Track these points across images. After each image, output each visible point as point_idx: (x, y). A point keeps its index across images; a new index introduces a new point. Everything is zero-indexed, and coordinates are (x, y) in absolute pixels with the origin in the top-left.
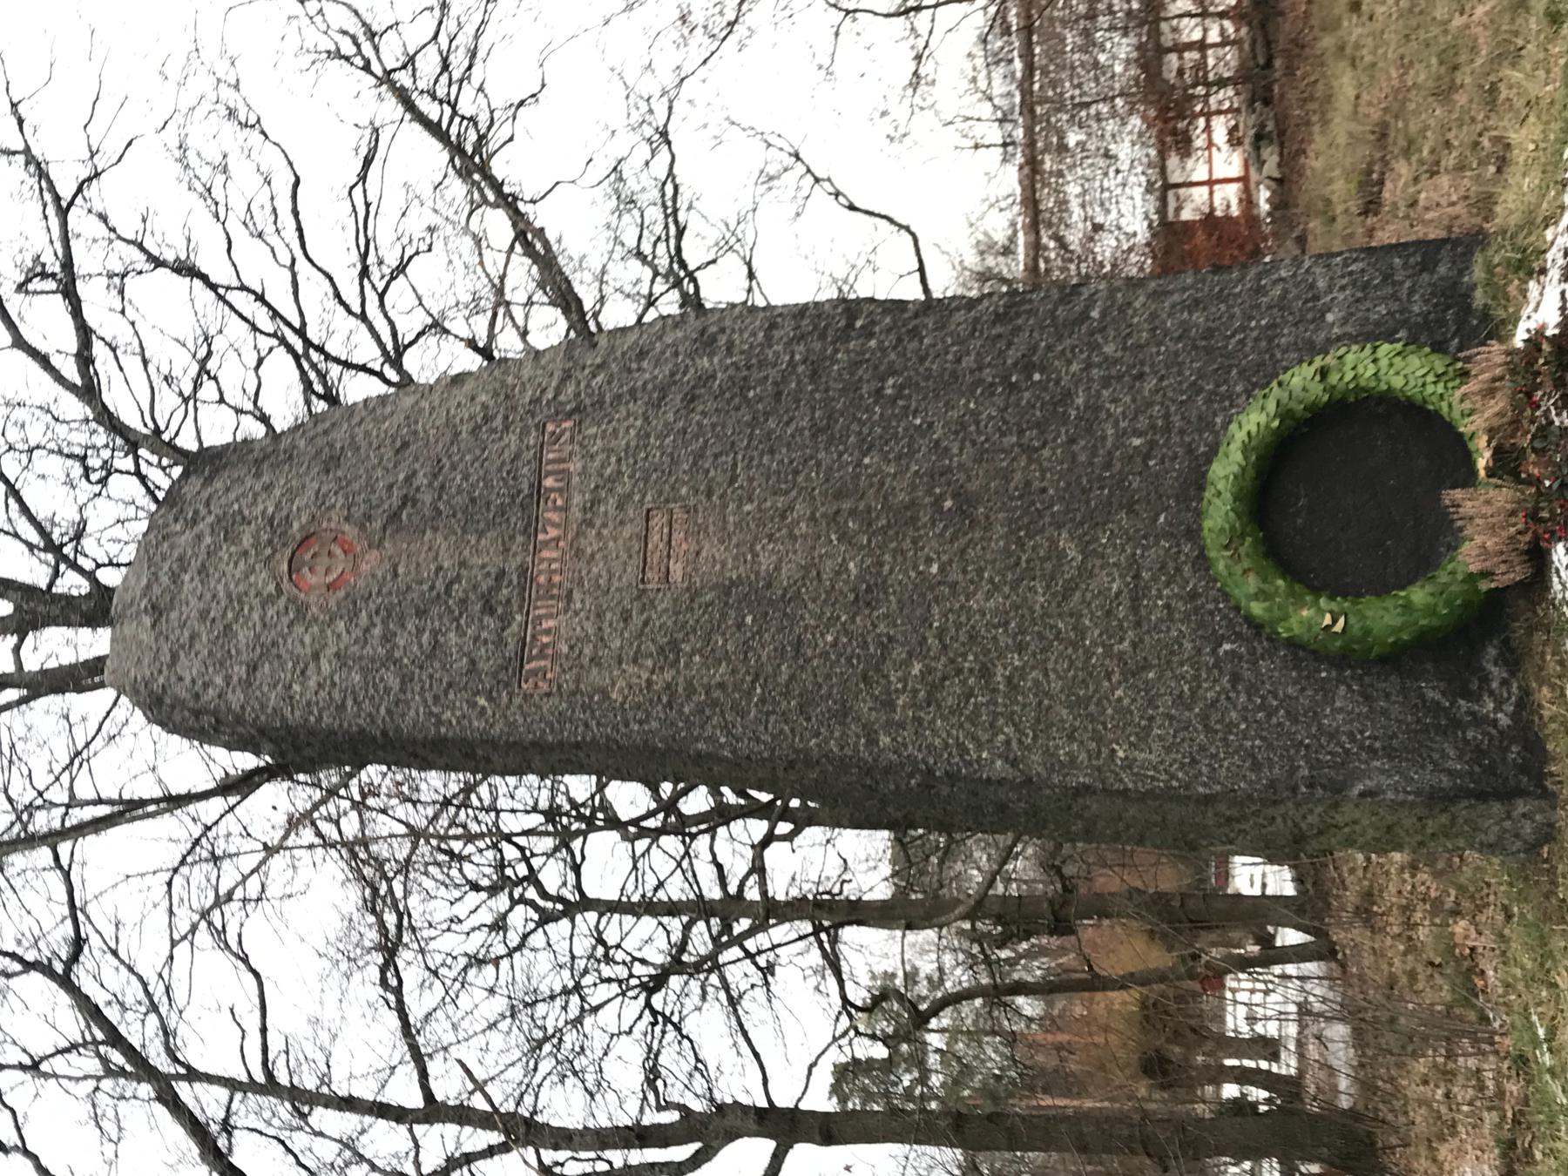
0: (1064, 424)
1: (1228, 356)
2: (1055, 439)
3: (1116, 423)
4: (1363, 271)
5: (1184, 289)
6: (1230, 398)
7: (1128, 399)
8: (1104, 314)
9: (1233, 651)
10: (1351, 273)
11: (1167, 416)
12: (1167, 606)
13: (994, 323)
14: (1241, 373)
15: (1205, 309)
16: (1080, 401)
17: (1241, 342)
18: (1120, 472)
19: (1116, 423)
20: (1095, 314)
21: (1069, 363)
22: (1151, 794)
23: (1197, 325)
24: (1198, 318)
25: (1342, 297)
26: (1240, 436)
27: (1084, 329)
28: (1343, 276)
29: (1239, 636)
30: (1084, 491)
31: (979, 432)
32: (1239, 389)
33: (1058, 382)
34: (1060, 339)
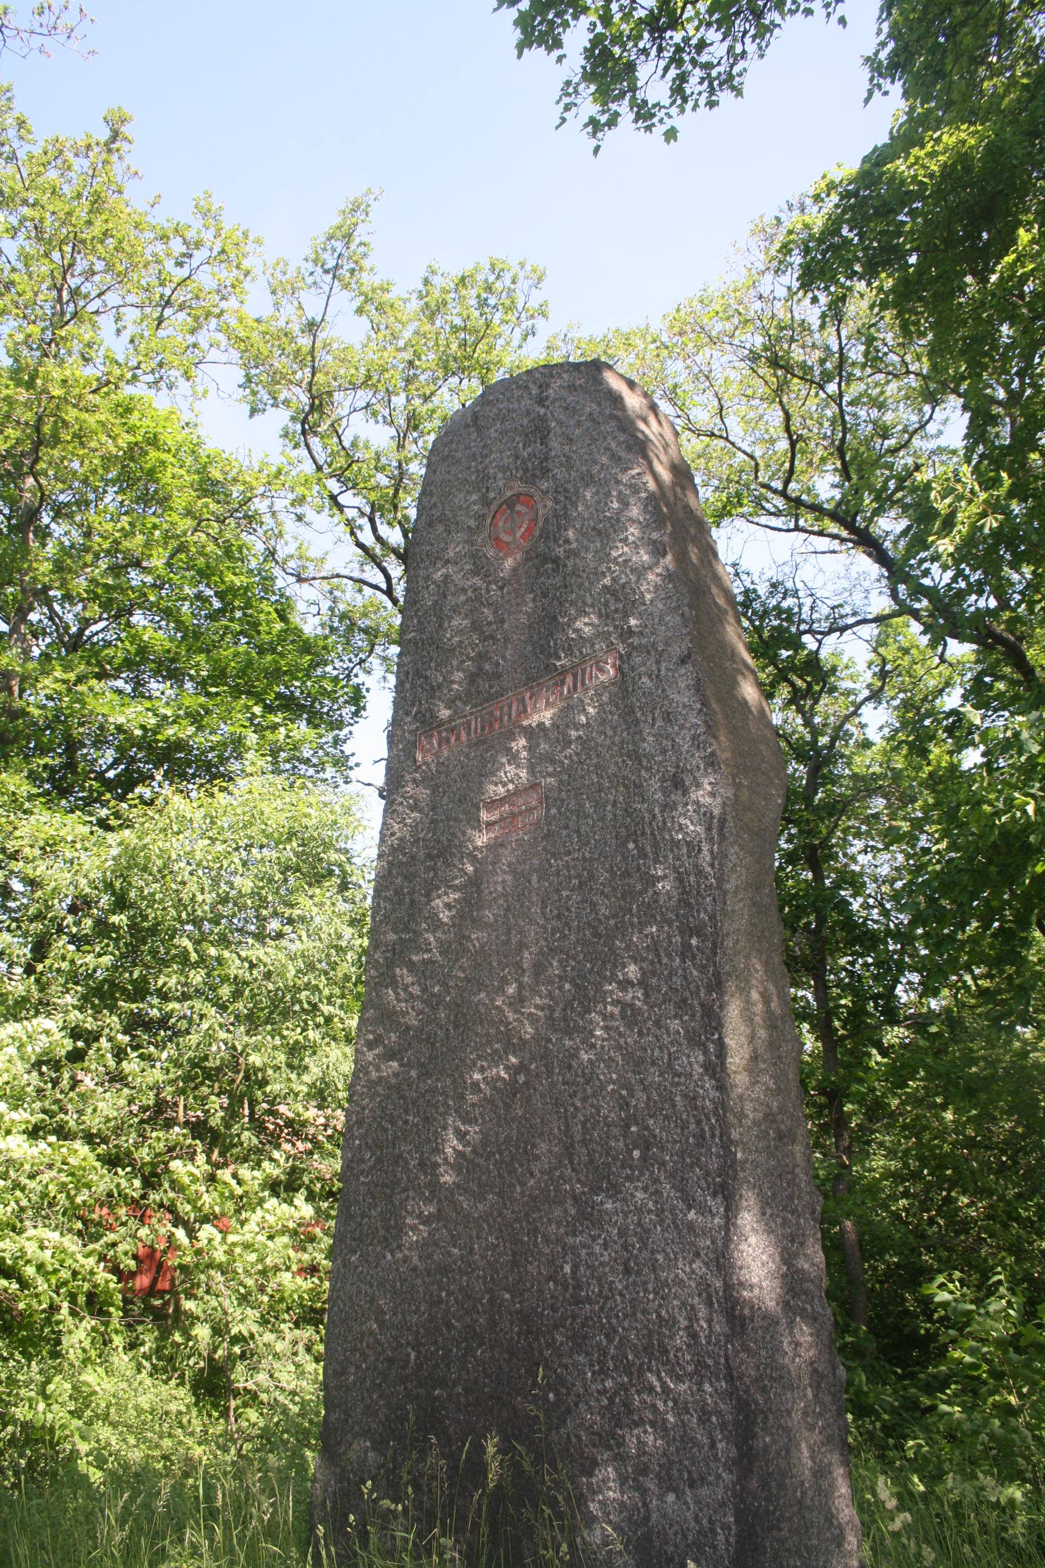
0: (591, 1189)
1: (641, 1372)
2: (579, 1181)
3: (584, 1246)
4: (715, 1548)
5: (709, 1321)
6: (602, 1371)
7: (606, 1258)
8: (691, 1226)
9: (408, 1362)
10: (713, 1530)
11: (588, 1300)
12: (440, 1301)
13: (685, 1096)
14: (623, 1387)
15: (689, 1346)
16: (609, 1206)
17: (651, 1389)
18: (540, 1253)
19: (584, 1246)
20: (692, 1215)
21: (645, 1189)
22: (517, 793)
23: (671, 1337)
24: (680, 1339)
25: (689, 1515)
26: (852, 1541)
27: (681, 1205)
28: (710, 1521)
29: (419, 1367)
30: (527, 1215)
31: (584, 1099)
32: (609, 1383)
33: (628, 1178)
34: (671, 1176)
